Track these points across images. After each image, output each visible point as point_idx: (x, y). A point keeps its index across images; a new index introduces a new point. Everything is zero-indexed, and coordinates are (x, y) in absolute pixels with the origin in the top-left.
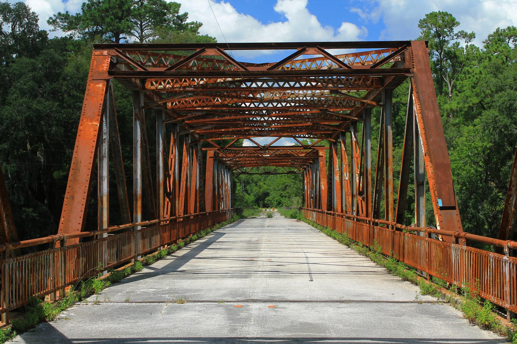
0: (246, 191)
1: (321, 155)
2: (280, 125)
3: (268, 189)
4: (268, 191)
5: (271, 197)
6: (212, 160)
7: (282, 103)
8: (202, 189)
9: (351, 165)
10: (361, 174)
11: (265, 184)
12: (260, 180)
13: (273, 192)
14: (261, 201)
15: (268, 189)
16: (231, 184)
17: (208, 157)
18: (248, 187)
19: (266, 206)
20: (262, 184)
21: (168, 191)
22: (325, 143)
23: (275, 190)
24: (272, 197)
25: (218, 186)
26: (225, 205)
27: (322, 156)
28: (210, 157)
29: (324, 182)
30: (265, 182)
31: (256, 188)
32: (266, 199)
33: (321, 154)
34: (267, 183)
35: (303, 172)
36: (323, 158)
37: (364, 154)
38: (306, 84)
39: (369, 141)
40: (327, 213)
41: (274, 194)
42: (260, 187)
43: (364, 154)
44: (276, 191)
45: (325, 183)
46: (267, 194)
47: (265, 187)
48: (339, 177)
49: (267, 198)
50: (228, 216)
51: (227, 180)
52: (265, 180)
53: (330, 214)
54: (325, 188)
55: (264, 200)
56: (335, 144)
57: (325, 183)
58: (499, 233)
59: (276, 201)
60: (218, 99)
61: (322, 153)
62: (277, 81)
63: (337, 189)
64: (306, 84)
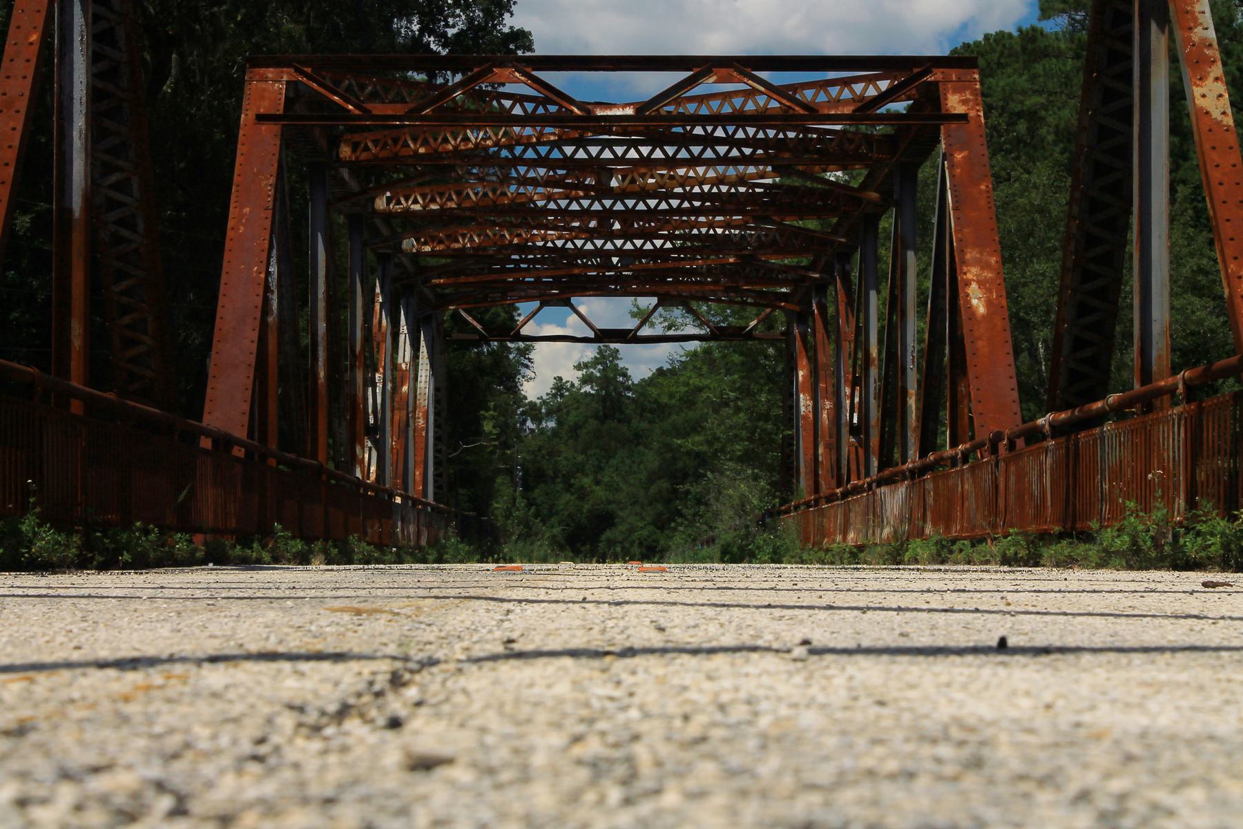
1: (960, 109)
2: (655, 262)
3: (610, 503)
4: (612, 507)
5: (620, 528)
6: (270, 132)
11: (598, 483)
12: (580, 469)
13: (627, 511)
14: (584, 545)
15: (610, 503)
16: (437, 389)
17: (246, 117)
20: (587, 481)
23: (635, 502)
24: (623, 527)
27: (963, 117)
28: (261, 118)
29: (985, 266)
30: (599, 477)
31: (568, 497)
32: (604, 537)
33: (954, 103)
34: (606, 479)
35: (788, 334)
36: (972, 125)
38: (729, 151)
41: (632, 519)
42: (583, 495)
44: (637, 508)
45: (988, 275)
47: (600, 492)
48: (1221, 88)
49: (608, 534)
52: (599, 469)
54: (989, 304)
57: (988, 275)
59: (641, 544)
60: (416, 197)
61: (964, 102)
62: (635, 144)
63: (943, 437)
64: (729, 151)
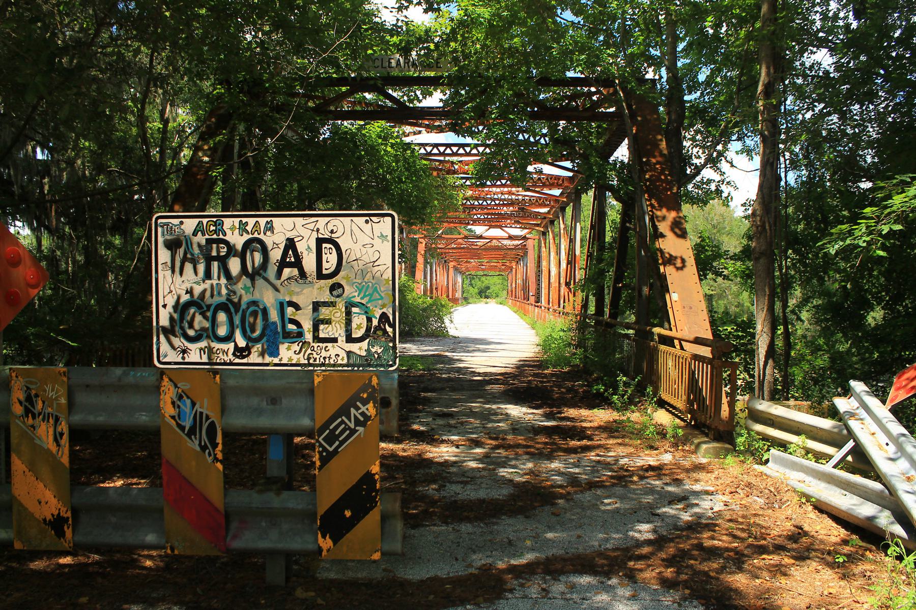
0: (471, 285)
7: (464, 152)
8: (579, 450)
9: (558, 253)
10: (569, 263)
18: (473, 282)
19: (487, 297)
21: (606, 501)
22: (534, 235)
25: (455, 284)
26: (458, 295)
37: (572, 241)
39: (578, 224)
40: (535, 306)
43: (572, 241)
46: (488, 288)
47: (487, 282)
50: (460, 302)
51: (459, 280)
53: (538, 306)
55: (486, 292)
56: (544, 234)
58: (579, 75)
